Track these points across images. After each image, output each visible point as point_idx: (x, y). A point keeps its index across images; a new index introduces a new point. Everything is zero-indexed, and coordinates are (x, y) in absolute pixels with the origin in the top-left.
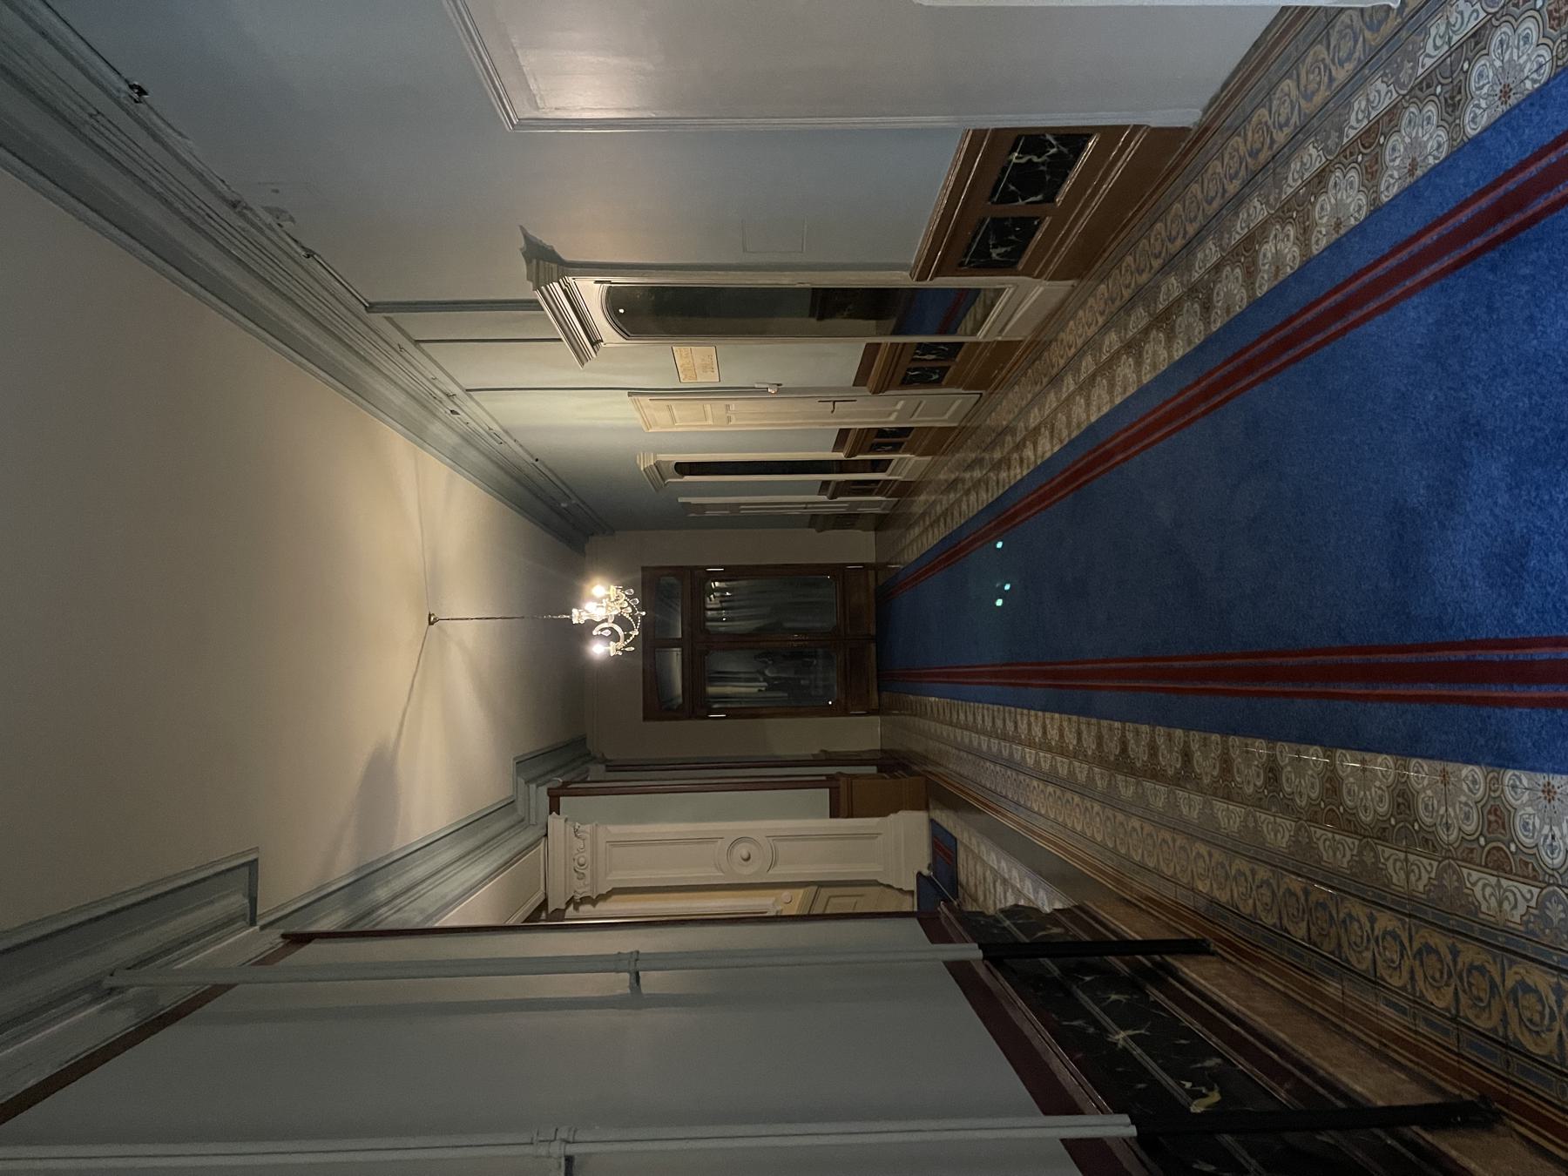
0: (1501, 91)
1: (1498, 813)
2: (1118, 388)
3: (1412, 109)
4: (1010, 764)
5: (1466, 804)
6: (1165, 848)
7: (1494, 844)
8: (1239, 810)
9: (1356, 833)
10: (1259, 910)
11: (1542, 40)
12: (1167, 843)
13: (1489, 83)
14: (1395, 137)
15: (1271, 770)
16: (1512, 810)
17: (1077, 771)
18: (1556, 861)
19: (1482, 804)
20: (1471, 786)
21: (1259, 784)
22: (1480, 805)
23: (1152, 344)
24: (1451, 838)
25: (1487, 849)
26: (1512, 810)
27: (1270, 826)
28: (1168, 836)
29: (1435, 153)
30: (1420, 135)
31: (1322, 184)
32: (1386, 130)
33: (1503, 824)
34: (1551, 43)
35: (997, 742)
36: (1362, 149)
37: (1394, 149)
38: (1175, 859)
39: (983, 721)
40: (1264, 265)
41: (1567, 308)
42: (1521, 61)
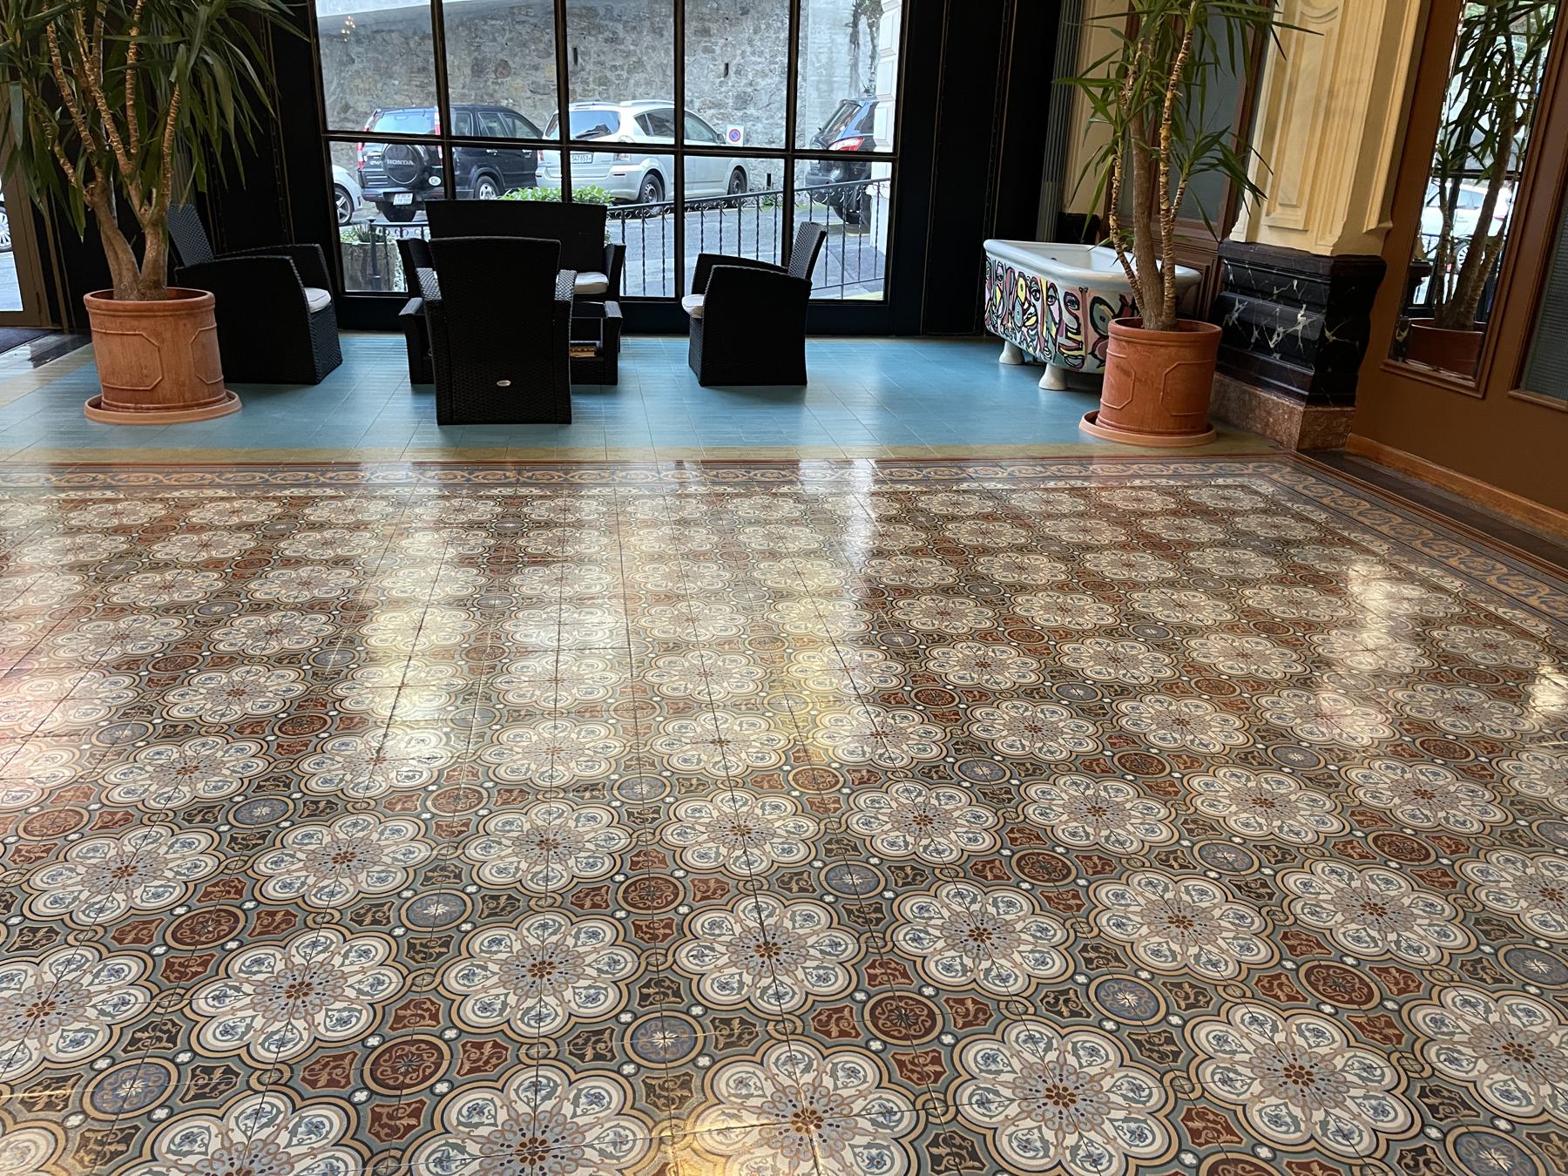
0: (1184, 917)
1: (362, 911)
3: (1268, 716)
4: (1115, 459)
11: (1223, 1017)
13: (1167, 943)
16: (499, 1085)
18: (202, 1002)
26: (499, 1085)
29: (1113, 839)
30: (1133, 821)
34: (1241, 978)
36: (1016, 857)
37: (1074, 834)
40: (972, 679)
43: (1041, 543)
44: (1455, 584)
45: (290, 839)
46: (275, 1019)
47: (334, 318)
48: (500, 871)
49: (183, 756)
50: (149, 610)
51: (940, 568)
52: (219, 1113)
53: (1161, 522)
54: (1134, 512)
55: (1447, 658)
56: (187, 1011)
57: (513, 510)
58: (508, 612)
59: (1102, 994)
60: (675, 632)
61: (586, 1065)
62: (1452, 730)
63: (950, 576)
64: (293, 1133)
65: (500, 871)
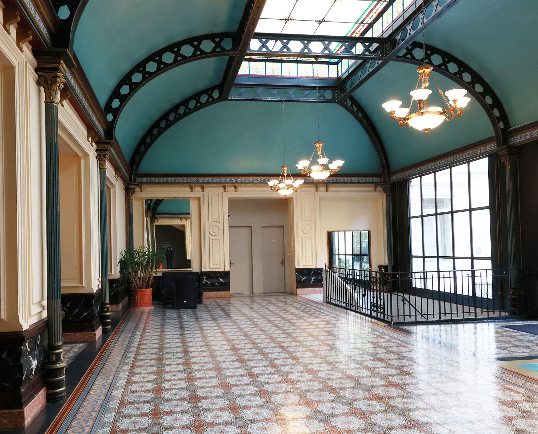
2: (310, 383)
6: (91, 409)
8: (116, 407)
9: (114, 422)
10: (73, 428)
12: (94, 409)
17: (122, 382)
21: (125, 412)
23: (318, 384)
27: (106, 431)
28: (97, 409)
31: (360, 418)
32: (359, 417)
35: (135, 350)
38: (79, 426)
39: (149, 326)
43: (358, 385)
44: (523, 391)
47: (25, 338)
51: (276, 400)
53: (396, 377)
54: (387, 375)
55: (524, 412)
57: (191, 383)
58: (119, 420)
60: (212, 420)
62: (531, 431)
63: (332, 397)
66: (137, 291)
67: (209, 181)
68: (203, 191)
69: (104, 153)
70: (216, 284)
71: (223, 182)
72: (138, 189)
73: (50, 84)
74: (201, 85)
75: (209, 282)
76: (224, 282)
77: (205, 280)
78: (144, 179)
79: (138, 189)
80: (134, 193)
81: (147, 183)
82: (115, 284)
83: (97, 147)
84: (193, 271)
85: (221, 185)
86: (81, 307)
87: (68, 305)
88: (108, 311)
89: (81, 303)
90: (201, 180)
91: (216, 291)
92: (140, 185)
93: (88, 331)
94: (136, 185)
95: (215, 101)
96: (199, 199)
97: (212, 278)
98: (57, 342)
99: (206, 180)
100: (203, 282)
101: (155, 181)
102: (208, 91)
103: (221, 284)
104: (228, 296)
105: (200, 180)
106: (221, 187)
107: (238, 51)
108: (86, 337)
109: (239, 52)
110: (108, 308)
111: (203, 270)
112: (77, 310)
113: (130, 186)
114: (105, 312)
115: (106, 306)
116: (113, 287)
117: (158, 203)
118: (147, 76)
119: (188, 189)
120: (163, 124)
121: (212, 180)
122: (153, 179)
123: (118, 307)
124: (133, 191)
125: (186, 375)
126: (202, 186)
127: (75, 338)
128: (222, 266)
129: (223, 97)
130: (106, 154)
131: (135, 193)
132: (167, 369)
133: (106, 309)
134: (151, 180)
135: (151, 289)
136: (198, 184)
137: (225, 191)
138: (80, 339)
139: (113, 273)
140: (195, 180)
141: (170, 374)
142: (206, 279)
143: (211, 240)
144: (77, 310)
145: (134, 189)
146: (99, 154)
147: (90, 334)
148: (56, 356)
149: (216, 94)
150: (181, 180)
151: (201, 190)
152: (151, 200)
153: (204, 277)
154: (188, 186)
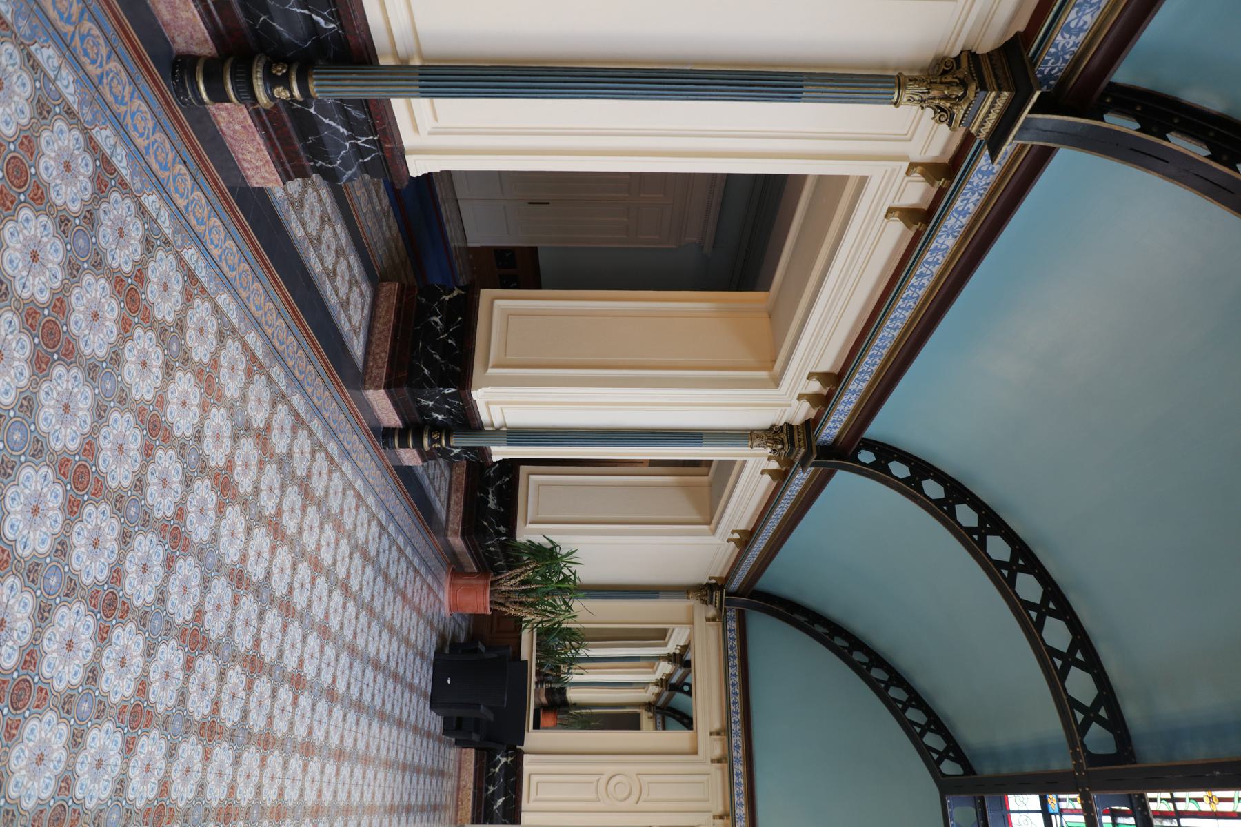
5: (78, 666)
7: (24, 677)
14: (28, 93)
15: (103, 639)
16: (6, 513)
19: (31, 99)
20: (22, 754)
22: (21, 740)
24: (13, 579)
25: (17, 681)
26: (6, 513)
33: (35, 663)
41: (3, 801)
42: (32, 232)
45: (179, 465)
46: (75, 421)
48: (150, 594)
49: (241, 466)
50: (343, 500)
52: (28, 361)
56: (88, 358)
59: (22, 184)
61: (13, 475)
64: (8, 384)
65: (150, 594)
66: (487, 578)
67: (737, 775)
68: (712, 761)
69: (785, 440)
70: (491, 789)
71: (737, 811)
72: (712, 612)
73: (944, 80)
74: (971, 735)
75: (497, 770)
76: (495, 808)
77: (503, 760)
78: (734, 625)
79: (712, 612)
80: (704, 602)
81: (725, 630)
82: (504, 529)
83: (798, 426)
84: (526, 733)
85: (728, 809)
86: (443, 365)
87: (450, 341)
88: (432, 441)
89: (450, 365)
90: (739, 756)
91: (475, 788)
92: (720, 618)
93: (389, 376)
94: (721, 609)
95: (933, 767)
96: (695, 752)
97: (506, 778)
98: (317, 85)
99: (739, 768)
100: (498, 757)
101: (732, 648)
102: (954, 750)
103: (490, 801)
104: (459, 817)
105: (738, 754)
106: (724, 806)
107: (1089, 769)
108: (375, 372)
109: (1087, 772)
110: (439, 441)
111: (526, 758)
112: (438, 357)
113: (718, 594)
114: (430, 436)
115: (443, 438)
116: (499, 526)
117: (686, 721)
118: (976, 537)
119: (717, 726)
120: (858, 656)
121: (740, 784)
122: (735, 643)
123: (456, 533)
124: (707, 599)
125: (326, 804)
126: (726, 759)
127: (378, 351)
128: (533, 805)
129: (946, 786)
130: (783, 444)
131: (704, 606)
132: (345, 770)
133: (436, 437)
134: (733, 639)
135: (489, 613)
136: (730, 747)
137: (714, 817)
138: (375, 359)
139: (529, 526)
140: (738, 740)
141: (333, 774)
142: (506, 763)
143: (595, 778)
144: (438, 357)
145: (711, 603)
146: (782, 431)
147: (381, 379)
148: (283, 74)
149: (949, 767)
150: (737, 708)
151: (714, 758)
152: (689, 693)
153: (510, 759)
154: (722, 725)
